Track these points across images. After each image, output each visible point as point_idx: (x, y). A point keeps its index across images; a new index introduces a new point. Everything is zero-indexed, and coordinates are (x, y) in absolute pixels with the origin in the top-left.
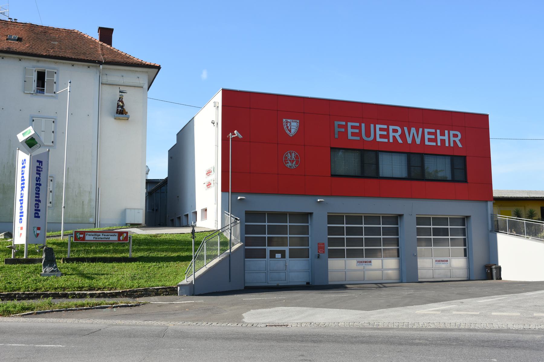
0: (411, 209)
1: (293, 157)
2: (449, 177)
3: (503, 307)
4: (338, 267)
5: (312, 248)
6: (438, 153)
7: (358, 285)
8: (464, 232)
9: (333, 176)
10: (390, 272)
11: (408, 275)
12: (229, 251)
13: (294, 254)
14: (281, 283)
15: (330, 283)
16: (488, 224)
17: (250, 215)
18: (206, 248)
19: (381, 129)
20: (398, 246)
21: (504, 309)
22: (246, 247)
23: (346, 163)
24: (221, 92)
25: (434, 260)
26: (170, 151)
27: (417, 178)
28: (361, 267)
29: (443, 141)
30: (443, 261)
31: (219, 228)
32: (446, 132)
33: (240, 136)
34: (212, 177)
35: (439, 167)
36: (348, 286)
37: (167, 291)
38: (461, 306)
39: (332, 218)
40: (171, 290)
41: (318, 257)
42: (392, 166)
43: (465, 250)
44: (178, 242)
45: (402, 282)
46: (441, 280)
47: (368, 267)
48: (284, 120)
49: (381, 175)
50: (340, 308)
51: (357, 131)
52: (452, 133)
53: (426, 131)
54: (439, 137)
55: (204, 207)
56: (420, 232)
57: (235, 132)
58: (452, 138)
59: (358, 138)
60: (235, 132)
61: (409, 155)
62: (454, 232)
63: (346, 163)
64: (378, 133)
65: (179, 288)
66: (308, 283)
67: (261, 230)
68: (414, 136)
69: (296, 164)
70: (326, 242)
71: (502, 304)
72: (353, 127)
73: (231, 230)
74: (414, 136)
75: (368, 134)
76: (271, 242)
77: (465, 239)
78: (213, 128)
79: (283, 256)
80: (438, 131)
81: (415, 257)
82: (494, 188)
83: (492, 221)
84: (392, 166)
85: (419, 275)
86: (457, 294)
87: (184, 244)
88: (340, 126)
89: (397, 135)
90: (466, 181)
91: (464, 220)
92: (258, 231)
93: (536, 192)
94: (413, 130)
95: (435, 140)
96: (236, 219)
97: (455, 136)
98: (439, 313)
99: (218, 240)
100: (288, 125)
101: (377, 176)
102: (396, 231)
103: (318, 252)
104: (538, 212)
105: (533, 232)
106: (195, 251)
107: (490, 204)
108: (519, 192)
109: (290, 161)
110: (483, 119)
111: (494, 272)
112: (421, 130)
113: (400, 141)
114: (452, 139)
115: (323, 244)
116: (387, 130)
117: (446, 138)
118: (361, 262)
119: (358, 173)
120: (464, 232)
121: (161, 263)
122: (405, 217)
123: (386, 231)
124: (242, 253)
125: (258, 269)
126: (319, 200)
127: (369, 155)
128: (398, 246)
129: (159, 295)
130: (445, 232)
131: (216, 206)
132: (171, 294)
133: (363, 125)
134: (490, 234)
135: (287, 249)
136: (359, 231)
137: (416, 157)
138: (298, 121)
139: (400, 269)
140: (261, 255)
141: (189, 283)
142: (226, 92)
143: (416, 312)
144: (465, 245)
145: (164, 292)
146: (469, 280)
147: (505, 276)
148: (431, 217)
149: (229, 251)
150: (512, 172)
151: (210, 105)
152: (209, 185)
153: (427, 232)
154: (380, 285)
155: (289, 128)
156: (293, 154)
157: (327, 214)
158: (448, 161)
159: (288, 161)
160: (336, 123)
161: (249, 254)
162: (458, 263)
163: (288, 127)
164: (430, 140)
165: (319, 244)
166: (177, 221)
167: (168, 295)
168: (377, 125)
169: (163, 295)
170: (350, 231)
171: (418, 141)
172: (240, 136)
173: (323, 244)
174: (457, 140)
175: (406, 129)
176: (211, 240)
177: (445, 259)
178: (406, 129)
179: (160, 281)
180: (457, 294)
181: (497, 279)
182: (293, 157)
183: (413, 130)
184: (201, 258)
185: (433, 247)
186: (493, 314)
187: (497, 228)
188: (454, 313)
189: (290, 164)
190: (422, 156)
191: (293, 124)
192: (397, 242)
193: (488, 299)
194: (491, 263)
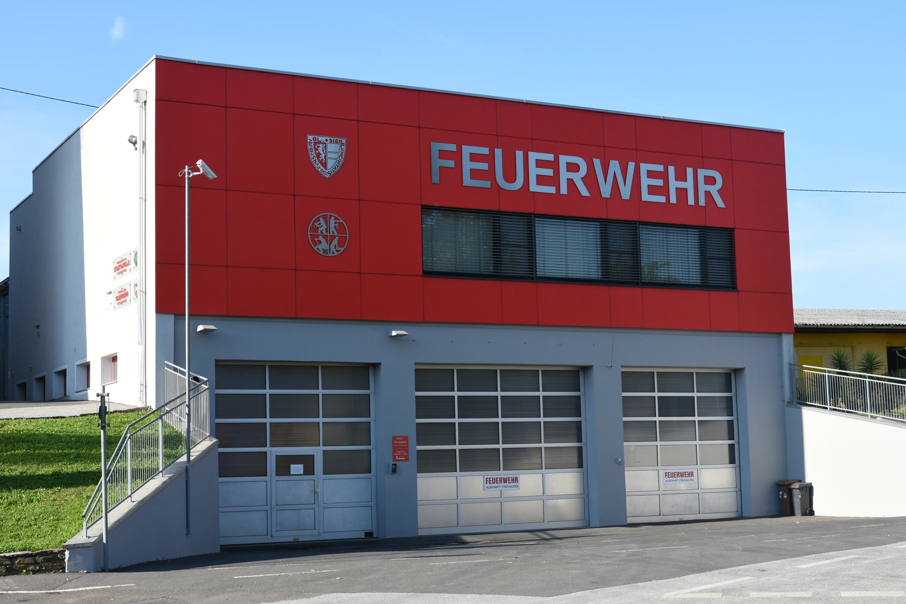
0: (610, 352)
1: (332, 229)
2: (694, 277)
3: (860, 578)
4: (443, 493)
5: (379, 449)
6: (671, 220)
7: (491, 537)
8: (729, 406)
9: (426, 273)
10: (561, 502)
11: (603, 509)
12: (184, 458)
13: (334, 465)
14: (305, 536)
15: (422, 533)
16: (782, 387)
17: (228, 371)
18: (132, 454)
19: (540, 164)
20: (580, 440)
21: (865, 582)
22: (625, 419)
23: (459, 244)
24: (153, 65)
25: (662, 473)
26: (11, 212)
27: (622, 283)
28: (494, 492)
29: (682, 193)
30: (682, 475)
31: (152, 403)
32: (690, 171)
33: (212, 175)
34: (132, 276)
35: (672, 256)
36: (468, 539)
37: (36, 563)
38: (763, 579)
39: (427, 376)
40: (49, 560)
41: (394, 471)
42: (567, 252)
43: (731, 447)
44: (51, 440)
45: (589, 527)
46: (677, 518)
47: (510, 492)
48: (310, 137)
49: (540, 272)
50: (481, 591)
51: (484, 166)
52: (702, 173)
53: (645, 167)
54: (674, 184)
55: (109, 352)
56: (630, 407)
57: (199, 163)
58: (703, 186)
59: (487, 184)
60: (199, 163)
61: (605, 224)
62: (707, 406)
63: (459, 244)
64: (534, 171)
65: (67, 553)
66: (369, 534)
67: (255, 406)
68: (617, 180)
69: (340, 244)
70: (412, 435)
71: (854, 572)
72: (474, 157)
73: (189, 406)
74: (617, 180)
75: (510, 176)
76: (283, 436)
77: (730, 423)
78: (132, 155)
79: (309, 470)
80: (671, 169)
81: (620, 465)
82: (797, 304)
83: (791, 378)
84: (567, 252)
85: (630, 509)
86: (744, 550)
87: (80, 445)
88: (443, 155)
89: (577, 177)
90: (733, 287)
91: (730, 378)
92: (249, 409)
93: (876, 313)
94: (614, 166)
95: (664, 191)
96: (196, 379)
97: (710, 181)
98: (720, 595)
99: (160, 432)
100: (320, 150)
101: (532, 277)
102: (575, 406)
103: (394, 459)
104: (882, 357)
105: (885, 405)
106: (107, 457)
107: (788, 340)
108: (840, 312)
109: (325, 237)
110: (772, 142)
111: (797, 498)
112: (631, 166)
113: (584, 192)
114: (703, 188)
115: (406, 438)
116: (555, 165)
117: (689, 185)
118: (495, 481)
119: (491, 269)
120: (729, 406)
121: (14, 491)
122: (596, 373)
123: (553, 406)
124: (214, 465)
125: (249, 503)
126: (394, 333)
127: (511, 224)
128: (580, 440)
129: (17, 572)
130: (686, 407)
131: (142, 348)
132: (48, 570)
133: (498, 152)
134: (788, 409)
135: (317, 452)
136: (488, 407)
137: (620, 229)
138: (344, 141)
139: (585, 496)
140: (256, 466)
141: (92, 540)
142: (167, 70)
143: (665, 595)
144: (731, 437)
145: (28, 565)
146: (741, 517)
147: (821, 507)
148: (655, 370)
149: (184, 458)
150: (840, 268)
151: (126, 96)
152: (122, 296)
153: (645, 406)
154: (542, 534)
155: (323, 156)
156: (332, 221)
157: (414, 367)
158: (693, 239)
159: (321, 238)
160: (436, 147)
161: (229, 466)
162: (716, 479)
163: (318, 155)
164: (652, 190)
165: (394, 438)
166: (35, 388)
167: (40, 571)
168: (531, 154)
169: (28, 573)
170: (468, 407)
171: (626, 192)
172: (212, 175)
173: (406, 438)
174: (714, 190)
175: (597, 162)
176: (144, 432)
177: (687, 469)
178: (597, 162)
179: (17, 537)
180: (744, 550)
181: (804, 514)
182: (332, 229)
183: (614, 166)
184: (117, 477)
185: (658, 443)
186: (844, 594)
187: (802, 396)
188: (754, 594)
189: (324, 245)
190: (634, 227)
191: (331, 147)
192: (577, 432)
193: (819, 559)
194: (791, 477)
